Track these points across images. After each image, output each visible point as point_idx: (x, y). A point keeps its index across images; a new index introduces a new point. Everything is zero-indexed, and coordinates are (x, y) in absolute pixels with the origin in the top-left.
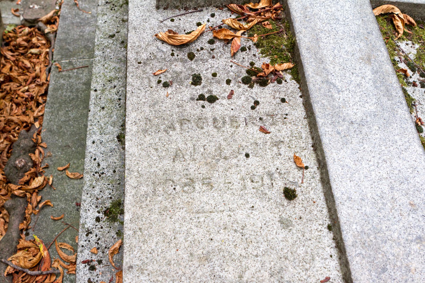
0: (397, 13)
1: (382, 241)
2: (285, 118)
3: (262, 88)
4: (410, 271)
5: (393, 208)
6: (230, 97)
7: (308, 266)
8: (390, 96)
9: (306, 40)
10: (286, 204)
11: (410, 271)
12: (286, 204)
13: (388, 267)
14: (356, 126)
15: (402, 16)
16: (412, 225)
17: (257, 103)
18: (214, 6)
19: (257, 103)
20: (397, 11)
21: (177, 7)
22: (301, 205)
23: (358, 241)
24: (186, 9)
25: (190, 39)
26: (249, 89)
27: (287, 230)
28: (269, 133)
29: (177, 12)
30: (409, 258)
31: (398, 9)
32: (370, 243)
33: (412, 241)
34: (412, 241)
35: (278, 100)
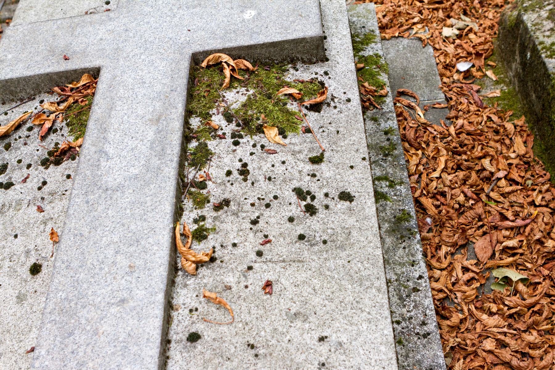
0: (224, 61)
1: (82, 306)
2: (64, 194)
3: (56, 167)
4: (97, 334)
5: (109, 272)
6: (25, 181)
7: (22, 338)
8: (162, 154)
9: (99, 111)
10: (29, 279)
11: (97, 334)
12: (29, 279)
13: (76, 332)
14: (109, 192)
15: (232, 62)
16: (121, 288)
17: (45, 183)
18: (45, 93)
19: (45, 183)
20: (225, 58)
21: (13, 100)
22: (41, 279)
23: (57, 308)
24: (22, 100)
25: (5, 130)
26: (44, 170)
27: (20, 305)
28: (44, 211)
29: (14, 104)
30: (102, 322)
31: (226, 56)
32: (68, 309)
33: (113, 304)
34: (113, 304)
35: (65, 177)
